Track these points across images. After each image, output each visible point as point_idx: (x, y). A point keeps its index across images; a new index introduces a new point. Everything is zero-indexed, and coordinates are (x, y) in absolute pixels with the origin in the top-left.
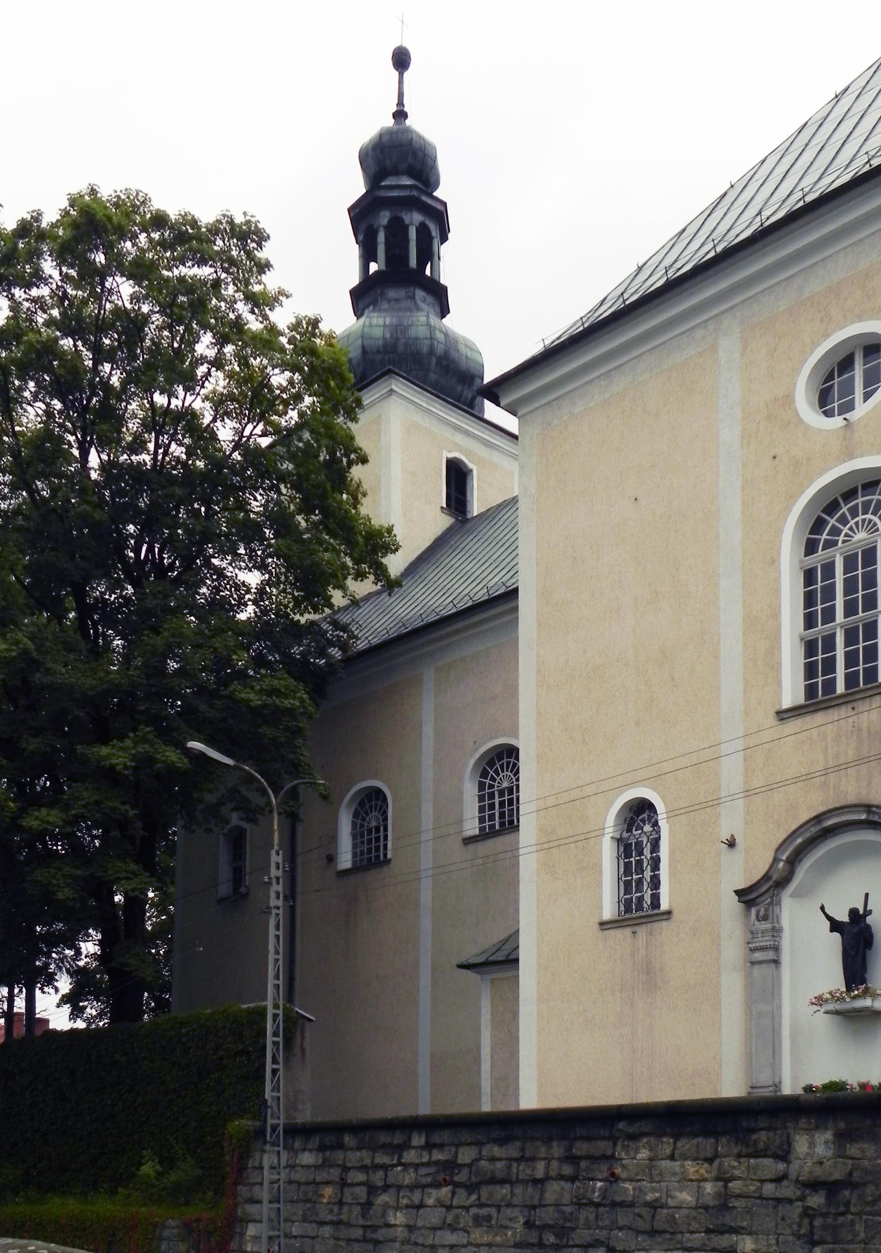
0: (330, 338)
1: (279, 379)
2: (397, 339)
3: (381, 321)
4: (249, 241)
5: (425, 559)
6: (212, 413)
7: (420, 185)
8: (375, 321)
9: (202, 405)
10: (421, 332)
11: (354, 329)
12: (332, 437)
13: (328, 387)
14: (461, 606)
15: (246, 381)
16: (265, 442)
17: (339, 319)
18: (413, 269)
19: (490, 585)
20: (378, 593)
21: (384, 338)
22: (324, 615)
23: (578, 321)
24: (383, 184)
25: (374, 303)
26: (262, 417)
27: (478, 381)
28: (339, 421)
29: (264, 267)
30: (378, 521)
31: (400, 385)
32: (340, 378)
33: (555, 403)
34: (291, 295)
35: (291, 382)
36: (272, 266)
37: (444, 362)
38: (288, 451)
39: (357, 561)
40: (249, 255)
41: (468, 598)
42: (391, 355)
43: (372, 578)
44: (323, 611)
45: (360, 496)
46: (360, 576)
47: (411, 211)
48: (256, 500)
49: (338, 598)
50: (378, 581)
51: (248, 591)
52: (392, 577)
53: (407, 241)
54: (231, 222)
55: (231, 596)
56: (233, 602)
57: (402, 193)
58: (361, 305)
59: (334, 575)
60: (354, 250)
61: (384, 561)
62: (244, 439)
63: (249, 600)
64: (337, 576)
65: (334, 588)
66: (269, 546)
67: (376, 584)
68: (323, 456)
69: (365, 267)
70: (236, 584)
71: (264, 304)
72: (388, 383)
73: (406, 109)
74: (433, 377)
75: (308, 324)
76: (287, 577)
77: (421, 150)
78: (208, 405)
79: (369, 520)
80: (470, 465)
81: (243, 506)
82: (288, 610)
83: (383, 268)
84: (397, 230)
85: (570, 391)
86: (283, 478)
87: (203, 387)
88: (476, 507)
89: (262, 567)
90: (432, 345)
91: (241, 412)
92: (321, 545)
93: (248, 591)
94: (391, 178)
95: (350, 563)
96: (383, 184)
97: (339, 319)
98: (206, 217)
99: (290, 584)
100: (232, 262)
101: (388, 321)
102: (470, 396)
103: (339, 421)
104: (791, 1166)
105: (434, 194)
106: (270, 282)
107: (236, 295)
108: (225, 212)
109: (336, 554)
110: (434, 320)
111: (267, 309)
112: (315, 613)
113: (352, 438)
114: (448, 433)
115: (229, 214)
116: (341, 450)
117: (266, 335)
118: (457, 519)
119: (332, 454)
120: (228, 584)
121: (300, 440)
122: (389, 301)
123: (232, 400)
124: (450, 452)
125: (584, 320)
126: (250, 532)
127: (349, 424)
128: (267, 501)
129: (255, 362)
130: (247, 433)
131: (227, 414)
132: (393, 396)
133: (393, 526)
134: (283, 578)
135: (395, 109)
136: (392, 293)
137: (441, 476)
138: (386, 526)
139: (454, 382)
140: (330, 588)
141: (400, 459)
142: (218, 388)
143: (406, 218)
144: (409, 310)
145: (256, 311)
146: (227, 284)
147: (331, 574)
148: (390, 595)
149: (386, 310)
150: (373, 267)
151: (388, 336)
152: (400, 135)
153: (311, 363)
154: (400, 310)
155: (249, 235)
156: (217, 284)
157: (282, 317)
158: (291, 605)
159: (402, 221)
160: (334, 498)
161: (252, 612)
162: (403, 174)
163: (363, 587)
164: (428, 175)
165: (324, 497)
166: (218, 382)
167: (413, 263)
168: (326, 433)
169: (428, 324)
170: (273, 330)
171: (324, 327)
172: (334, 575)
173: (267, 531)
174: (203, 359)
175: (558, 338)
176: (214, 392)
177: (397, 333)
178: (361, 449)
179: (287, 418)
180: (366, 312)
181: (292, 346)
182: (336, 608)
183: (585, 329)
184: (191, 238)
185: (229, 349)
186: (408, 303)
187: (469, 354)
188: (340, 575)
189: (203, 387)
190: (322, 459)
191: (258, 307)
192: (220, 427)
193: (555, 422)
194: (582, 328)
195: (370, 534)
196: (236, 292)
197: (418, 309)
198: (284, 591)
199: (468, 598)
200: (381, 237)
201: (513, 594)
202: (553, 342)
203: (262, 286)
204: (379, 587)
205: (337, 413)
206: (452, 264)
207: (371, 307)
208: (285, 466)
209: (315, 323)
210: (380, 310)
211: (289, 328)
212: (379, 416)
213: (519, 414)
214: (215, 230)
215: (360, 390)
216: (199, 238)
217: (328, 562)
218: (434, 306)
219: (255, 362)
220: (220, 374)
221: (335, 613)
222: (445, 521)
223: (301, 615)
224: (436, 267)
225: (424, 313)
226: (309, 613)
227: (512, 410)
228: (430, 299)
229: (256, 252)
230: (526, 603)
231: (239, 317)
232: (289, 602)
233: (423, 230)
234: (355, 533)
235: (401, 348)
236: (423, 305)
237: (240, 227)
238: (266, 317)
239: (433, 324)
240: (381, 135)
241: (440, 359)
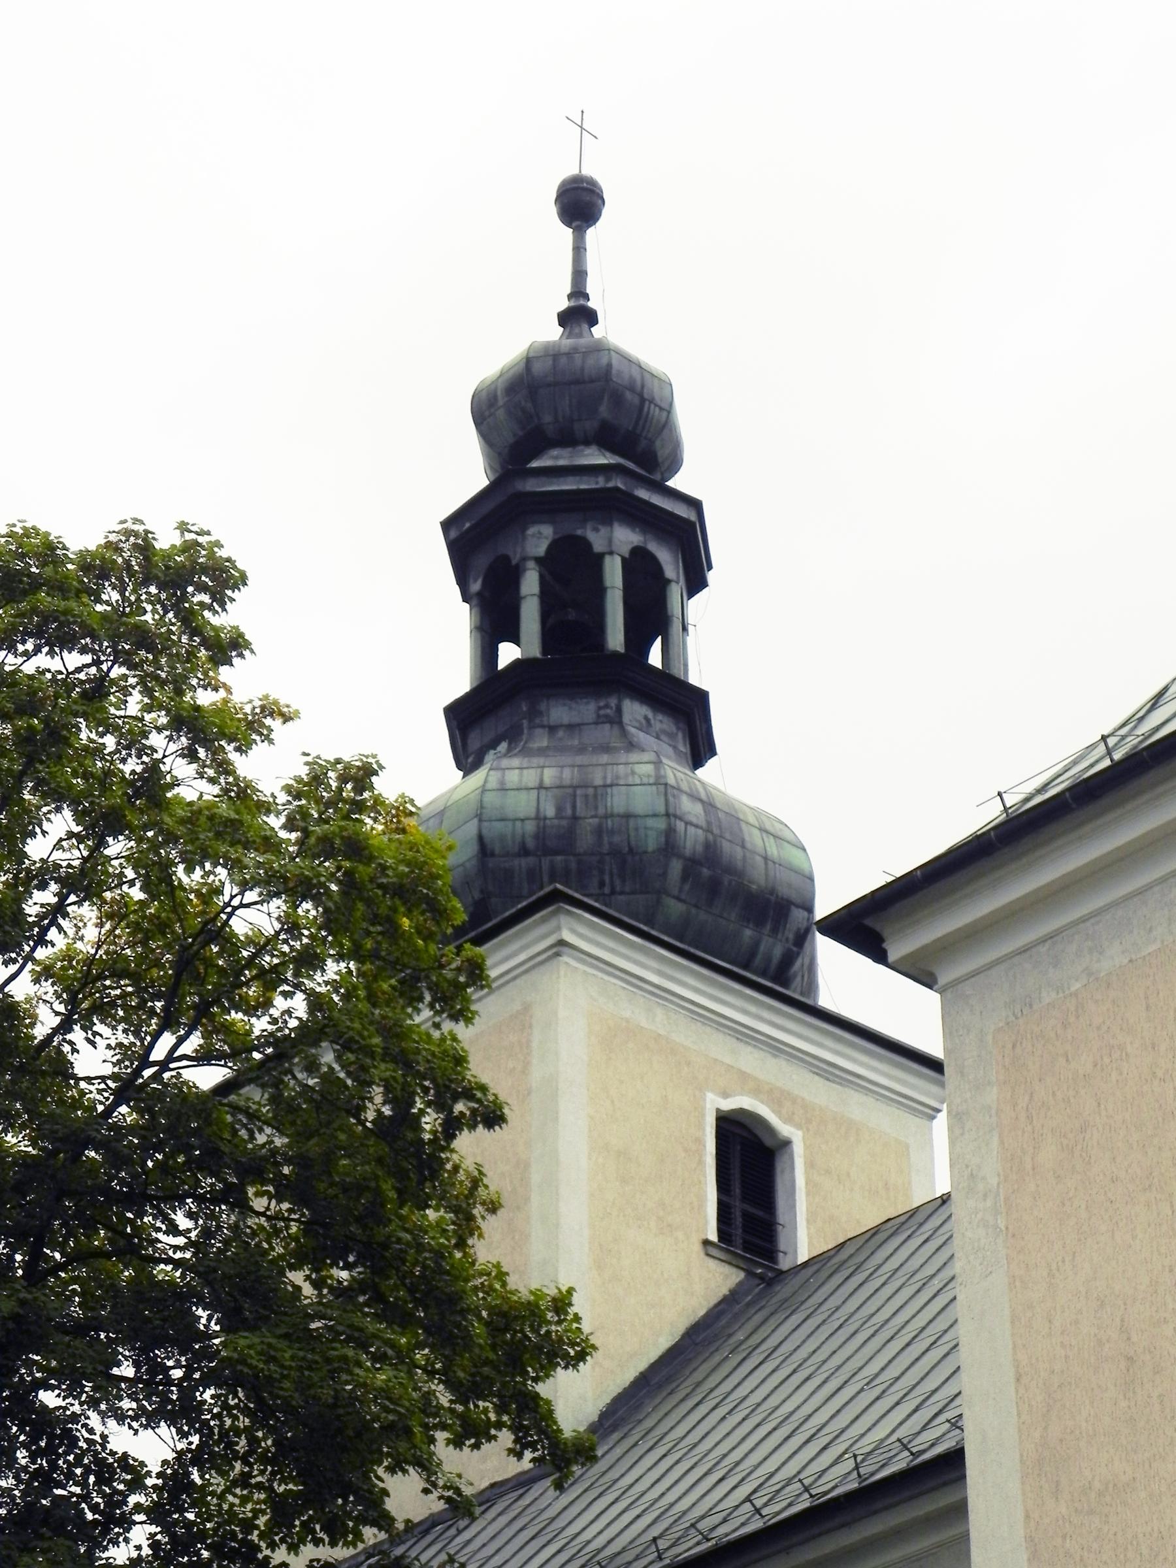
0: (402, 811)
1: (255, 918)
2: (575, 818)
3: (530, 777)
4: (190, 589)
5: (660, 1386)
6: (61, 1008)
7: (631, 465)
8: (513, 777)
9: (32, 989)
10: (642, 800)
11: (457, 796)
12: (404, 1060)
13: (392, 931)
14: (779, 1511)
15: (161, 926)
16: (207, 1077)
17: (421, 773)
18: (615, 654)
19: (864, 1446)
20: (522, 1482)
21: (539, 817)
23: (1092, 747)
24: (535, 464)
25: (512, 736)
26: (202, 1016)
27: (798, 915)
28: (418, 1019)
29: (228, 647)
30: (528, 1280)
31: (582, 930)
32: (415, 917)
33: (1043, 949)
34: (297, 713)
35: (291, 926)
36: (247, 645)
37: (706, 872)
38: (274, 1100)
39: (463, 1392)
40: (190, 621)
41: (796, 1487)
42: (559, 858)
43: (506, 1438)
44: (359, 1537)
45: (478, 1211)
46: (471, 1433)
47: (609, 523)
48: (173, 1230)
49: (406, 1496)
50: (525, 1446)
51: (136, 1484)
52: (568, 1433)
53: (599, 591)
54: (145, 547)
55: (86, 1497)
56: (90, 1516)
58: (475, 742)
59: (399, 1430)
60: (458, 618)
61: (543, 1389)
62: (147, 1073)
63: (138, 1508)
64: (408, 1432)
65: (391, 1470)
66: (208, 1353)
67: (519, 1456)
68: (377, 1105)
69: (487, 654)
70: (100, 1462)
71: (222, 735)
72: (553, 923)
74: (674, 908)
75: (343, 779)
76: (253, 1442)
77: (632, 388)
78: (48, 988)
79: (502, 1276)
80: (784, 1129)
81: (135, 1249)
82: (254, 1537)
83: (536, 652)
84: (572, 570)
85: (1083, 920)
86: (256, 1168)
87: (41, 941)
88: (804, 1237)
89: (182, 1413)
90: (670, 832)
91: (142, 1005)
92: (363, 1346)
93: (136, 1484)
94: (555, 452)
95: (444, 1398)
96: (535, 464)
97: (421, 773)
98: (81, 533)
99: (264, 1459)
100: (143, 638)
101: (549, 776)
102: (778, 952)
103: (418, 1019)
105: (670, 483)
106: (242, 683)
107: (148, 717)
108: (129, 525)
109: (398, 1373)
110: (675, 771)
111: (230, 748)
112: (333, 1544)
113: (460, 1060)
114: (720, 1047)
115: (140, 528)
116: (426, 1090)
117: (224, 810)
118: (749, 1273)
119: (401, 1100)
120: (78, 1462)
121: (312, 1067)
122: (552, 729)
123: (117, 975)
124: (725, 1095)
125: (1111, 741)
126: (154, 1319)
127: (448, 1026)
128: (206, 1233)
129: (188, 878)
130: (158, 1054)
131: (104, 1010)
132: (565, 959)
133: (570, 1291)
134: (242, 1444)
135: (564, 304)
136: (559, 712)
137: (701, 1162)
138: (552, 1292)
139: (732, 919)
140: (380, 1471)
141: (588, 1114)
142: (79, 945)
143: (597, 539)
144: (606, 749)
145: (202, 753)
146: (125, 691)
147: (389, 1428)
148: (559, 1486)
149: (542, 752)
150: (508, 653)
151: (550, 811)
152: (578, 358)
153: (349, 874)
154: (582, 750)
155: (194, 576)
156: (98, 690)
157: (269, 769)
158: (261, 1521)
159: (588, 545)
160: (401, 1218)
161: (145, 1544)
162: (587, 443)
163: (486, 1464)
164: (651, 442)
165: (375, 1214)
166: (84, 930)
167: (616, 638)
169: (660, 782)
170: (242, 795)
171: (386, 787)
172: (399, 1430)
173: (202, 1313)
174: (44, 874)
175: (1039, 791)
176: (68, 956)
177: (574, 807)
178: (483, 1088)
179: (275, 1013)
180: (490, 756)
181: (294, 836)
182: (400, 1526)
183: (1115, 765)
184: (36, 584)
185: (116, 847)
186: (606, 732)
187: (773, 850)
188: (417, 1430)
189: (41, 941)
190: (370, 1115)
191: (207, 743)
192: (81, 1044)
193: (1048, 996)
194: (1107, 763)
195: (504, 1315)
196: (148, 709)
197: (632, 746)
198: (244, 1480)
199: (796, 1487)
200: (530, 583)
201: (951, 1464)
202: (1027, 800)
203: (222, 693)
204: (526, 1464)
205: (414, 1000)
206: (713, 641)
207: (503, 747)
208: (261, 1139)
209: (362, 775)
210: (526, 752)
211: (288, 789)
212: (527, 1008)
213: (942, 980)
214: (99, 567)
215: (479, 941)
216: (60, 587)
217: (385, 1392)
218: (672, 736)
219: (188, 878)
220: (88, 912)
221: (395, 1539)
222: (718, 1279)
223: (293, 1548)
224: (674, 651)
225: (648, 756)
226: (317, 1542)
227: (920, 971)
228: (662, 722)
229: (206, 614)
230: (994, 1497)
231: (154, 769)
232: (256, 1513)
233: (640, 567)
234: (463, 1312)
235: (585, 840)
236: (641, 737)
237: (167, 556)
238: (225, 767)
239: (671, 780)
240: (529, 361)
241: (692, 865)
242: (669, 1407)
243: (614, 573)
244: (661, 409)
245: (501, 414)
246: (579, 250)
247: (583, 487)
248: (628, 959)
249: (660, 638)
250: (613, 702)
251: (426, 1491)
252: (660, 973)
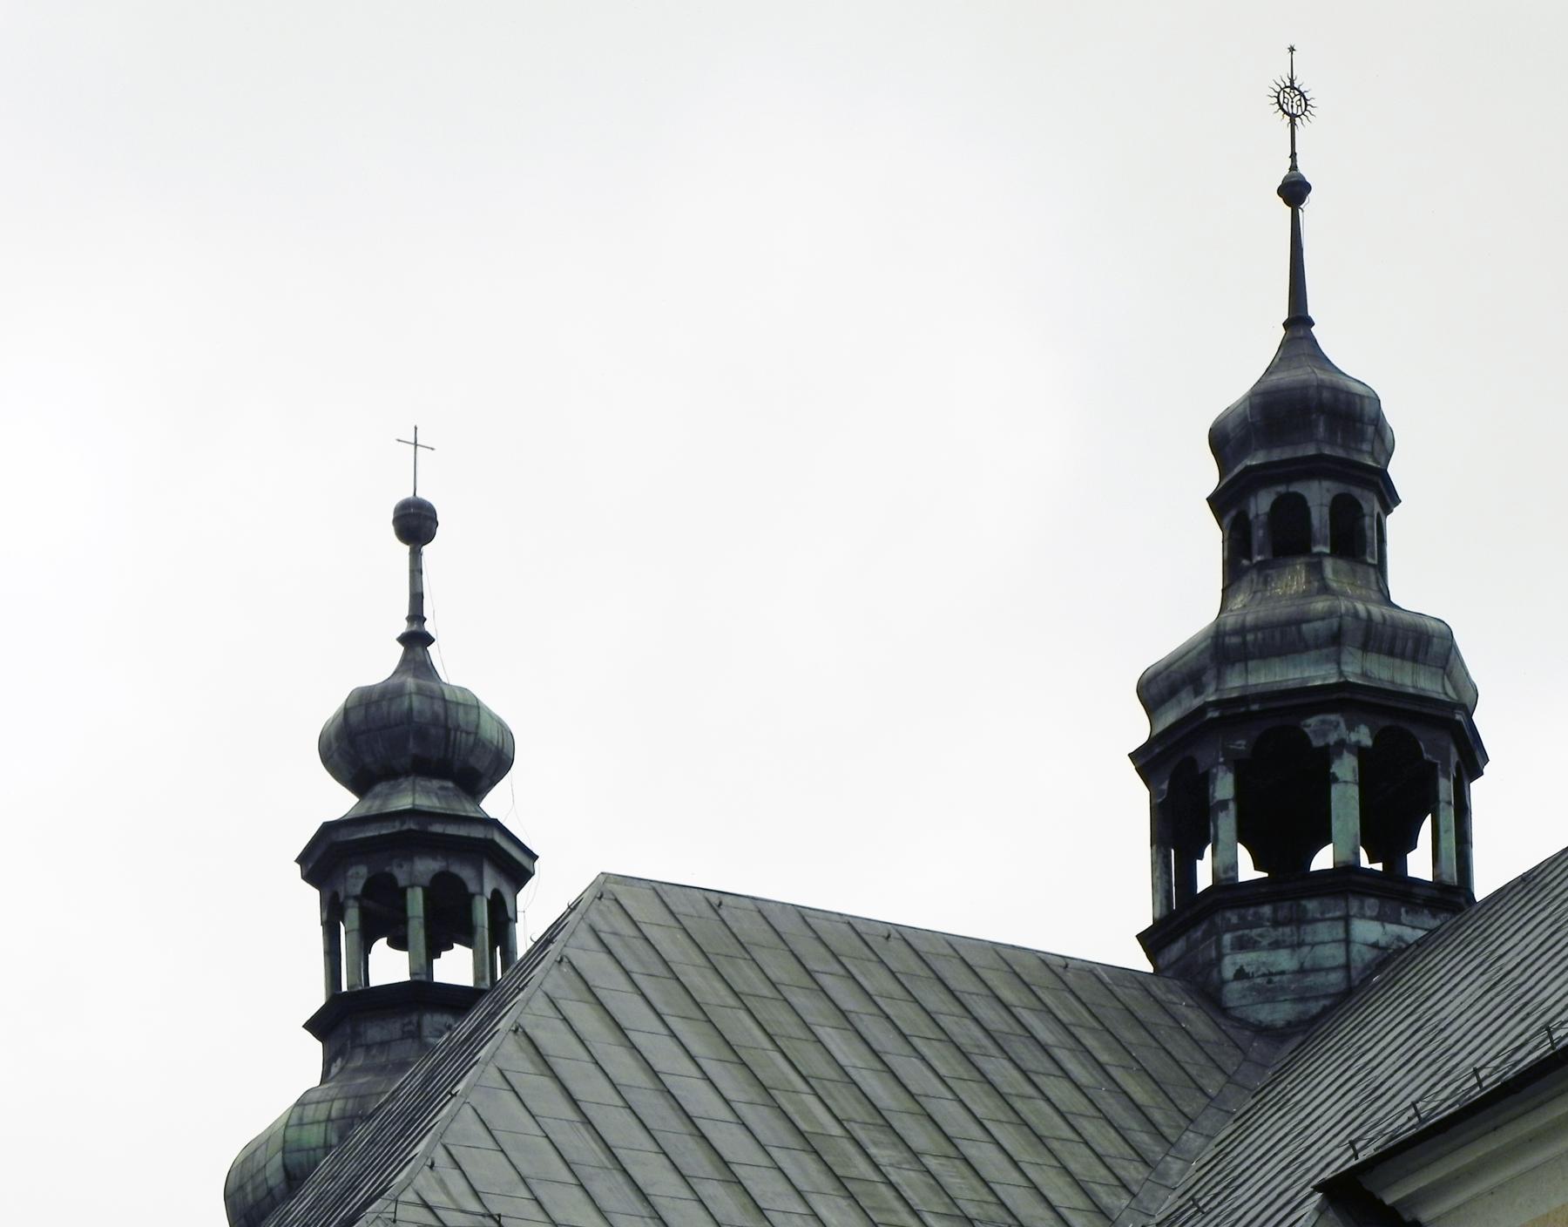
22: (1282, 489)
47: (410, 859)
57: (395, 827)
122: (368, 1047)
135: (403, 627)
143: (401, 876)
159: (392, 879)
186: (409, 1047)
240: (346, 711)
244: (468, 733)
245: (336, 756)
247: (384, 832)
249: (1429, 818)
250: (414, 1018)
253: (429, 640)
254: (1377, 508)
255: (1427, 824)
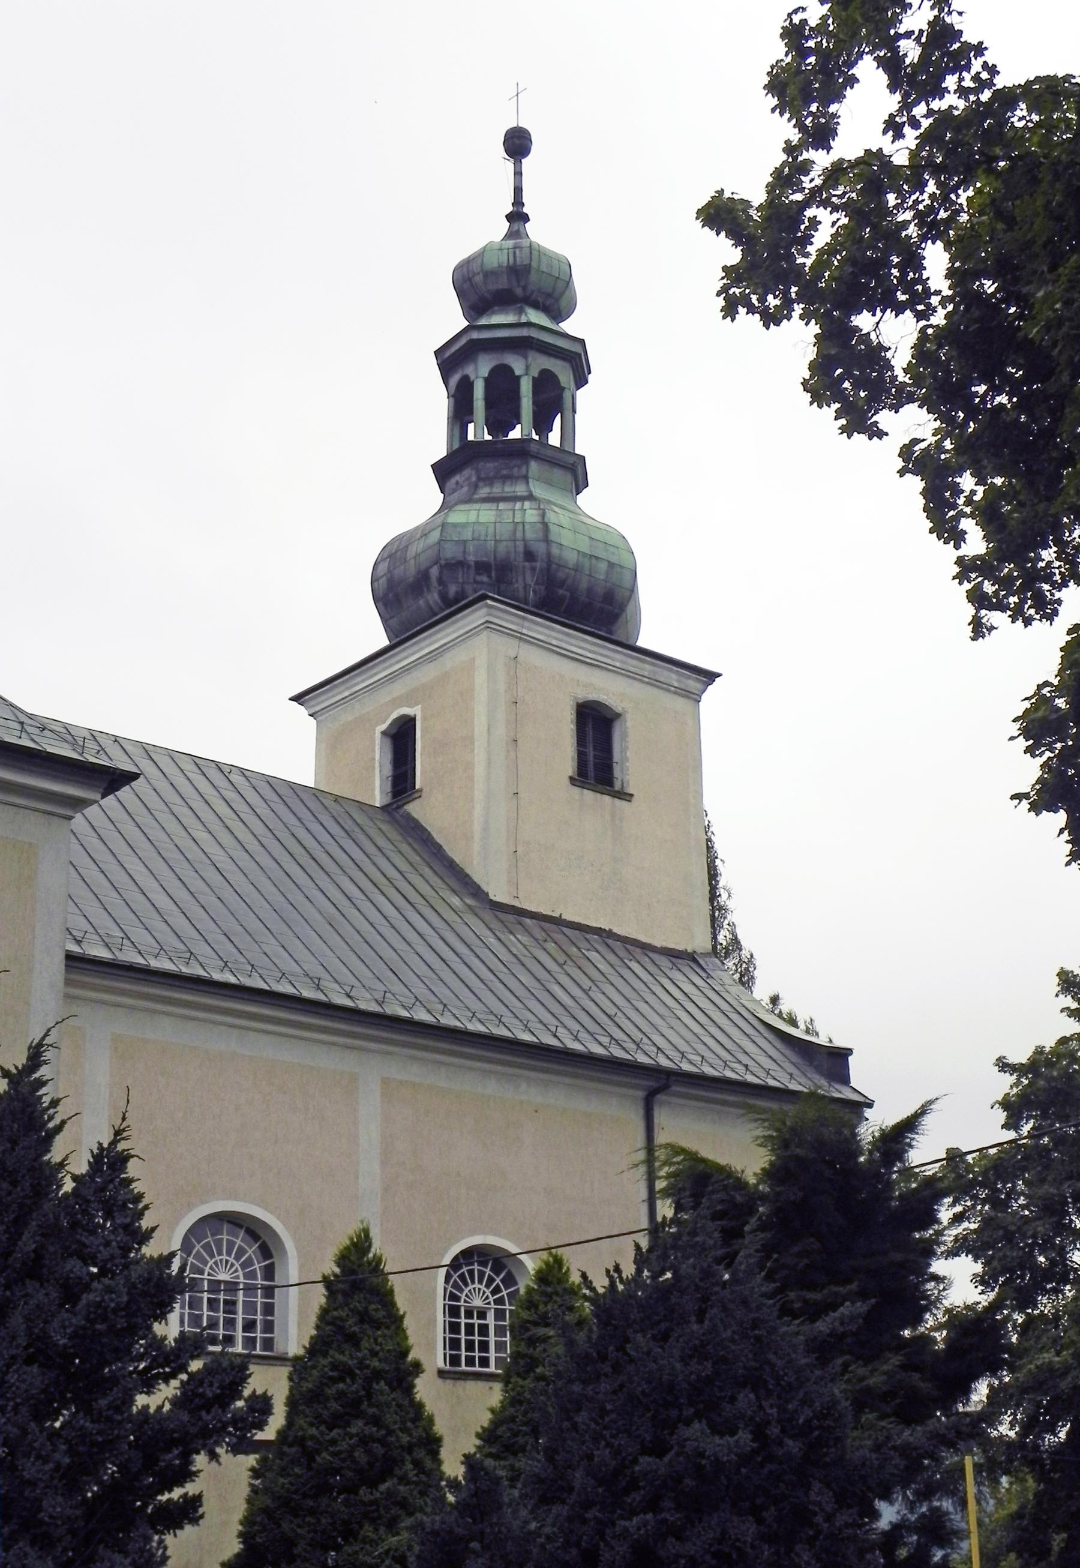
36: (858, 81)
73: (525, 210)
84: (502, 388)
104: (931, 15)
135: (510, 209)
159: (511, 370)
168: (482, 1547)
206: (596, 421)
233: (546, 383)
242: (313, 910)
243: (526, 387)
246: (518, 174)
248: (333, 696)
249: (559, 415)
251: (775, 1000)
252: (348, 689)
253: (526, 218)
254: (573, 385)
255: (558, 418)
